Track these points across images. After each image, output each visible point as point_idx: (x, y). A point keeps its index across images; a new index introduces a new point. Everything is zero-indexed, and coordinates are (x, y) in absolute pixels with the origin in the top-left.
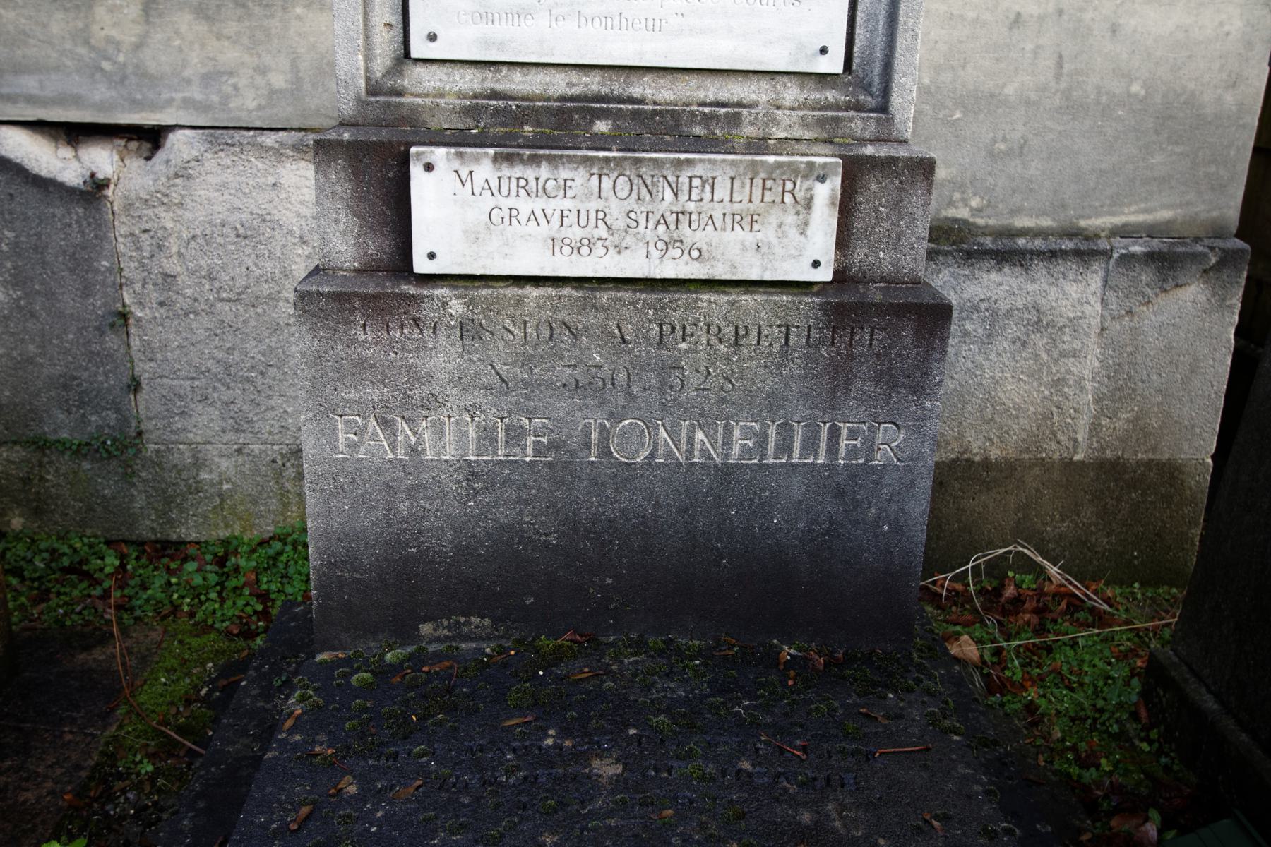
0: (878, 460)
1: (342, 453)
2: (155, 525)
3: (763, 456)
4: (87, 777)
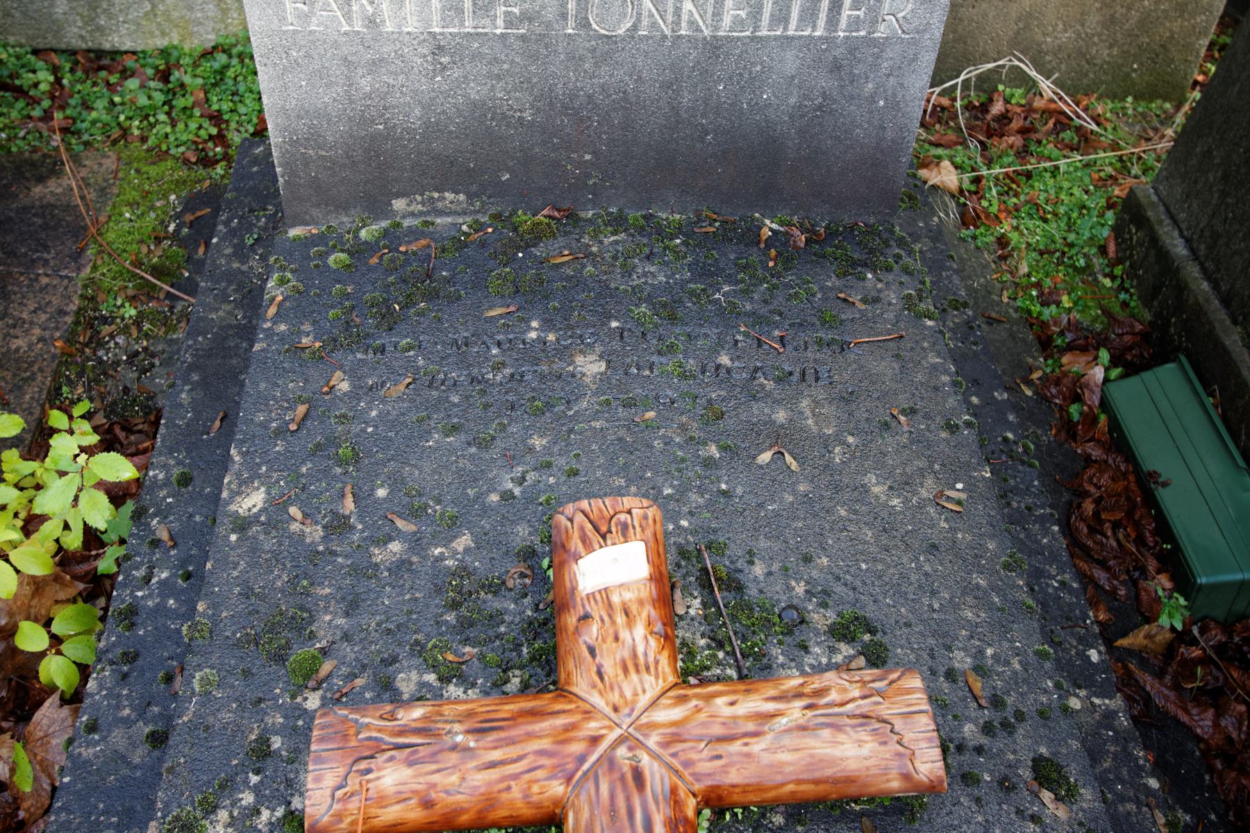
0: (881, 32)
1: (292, 24)
2: (83, 32)
3: (756, 28)
4: (73, 322)
